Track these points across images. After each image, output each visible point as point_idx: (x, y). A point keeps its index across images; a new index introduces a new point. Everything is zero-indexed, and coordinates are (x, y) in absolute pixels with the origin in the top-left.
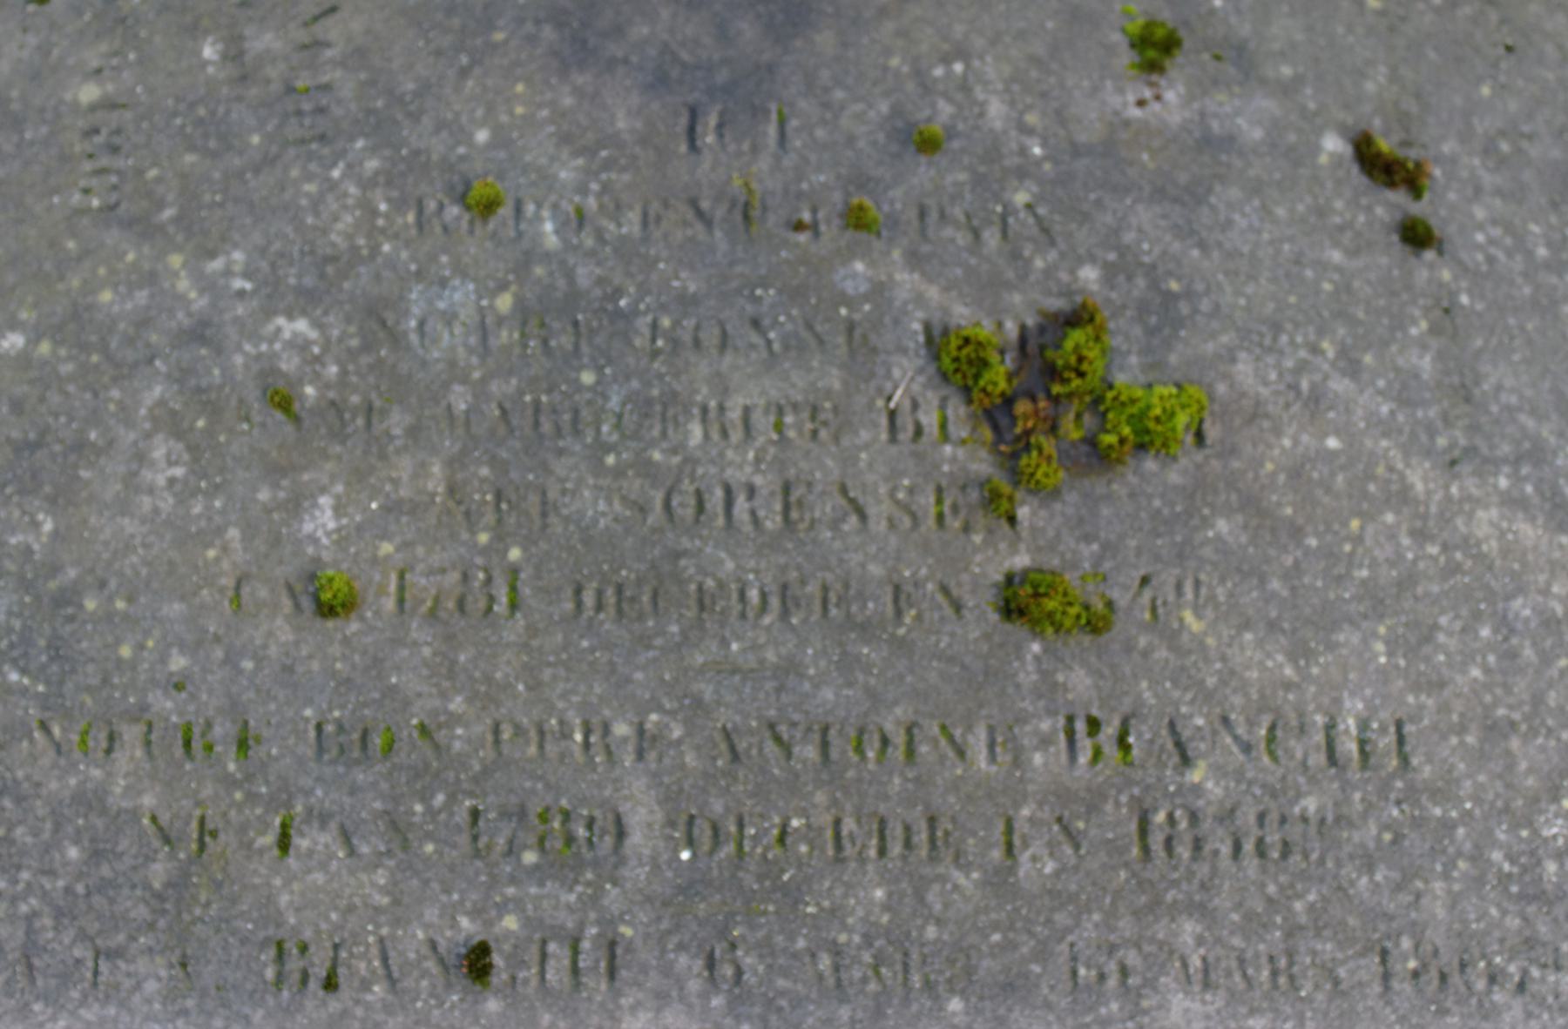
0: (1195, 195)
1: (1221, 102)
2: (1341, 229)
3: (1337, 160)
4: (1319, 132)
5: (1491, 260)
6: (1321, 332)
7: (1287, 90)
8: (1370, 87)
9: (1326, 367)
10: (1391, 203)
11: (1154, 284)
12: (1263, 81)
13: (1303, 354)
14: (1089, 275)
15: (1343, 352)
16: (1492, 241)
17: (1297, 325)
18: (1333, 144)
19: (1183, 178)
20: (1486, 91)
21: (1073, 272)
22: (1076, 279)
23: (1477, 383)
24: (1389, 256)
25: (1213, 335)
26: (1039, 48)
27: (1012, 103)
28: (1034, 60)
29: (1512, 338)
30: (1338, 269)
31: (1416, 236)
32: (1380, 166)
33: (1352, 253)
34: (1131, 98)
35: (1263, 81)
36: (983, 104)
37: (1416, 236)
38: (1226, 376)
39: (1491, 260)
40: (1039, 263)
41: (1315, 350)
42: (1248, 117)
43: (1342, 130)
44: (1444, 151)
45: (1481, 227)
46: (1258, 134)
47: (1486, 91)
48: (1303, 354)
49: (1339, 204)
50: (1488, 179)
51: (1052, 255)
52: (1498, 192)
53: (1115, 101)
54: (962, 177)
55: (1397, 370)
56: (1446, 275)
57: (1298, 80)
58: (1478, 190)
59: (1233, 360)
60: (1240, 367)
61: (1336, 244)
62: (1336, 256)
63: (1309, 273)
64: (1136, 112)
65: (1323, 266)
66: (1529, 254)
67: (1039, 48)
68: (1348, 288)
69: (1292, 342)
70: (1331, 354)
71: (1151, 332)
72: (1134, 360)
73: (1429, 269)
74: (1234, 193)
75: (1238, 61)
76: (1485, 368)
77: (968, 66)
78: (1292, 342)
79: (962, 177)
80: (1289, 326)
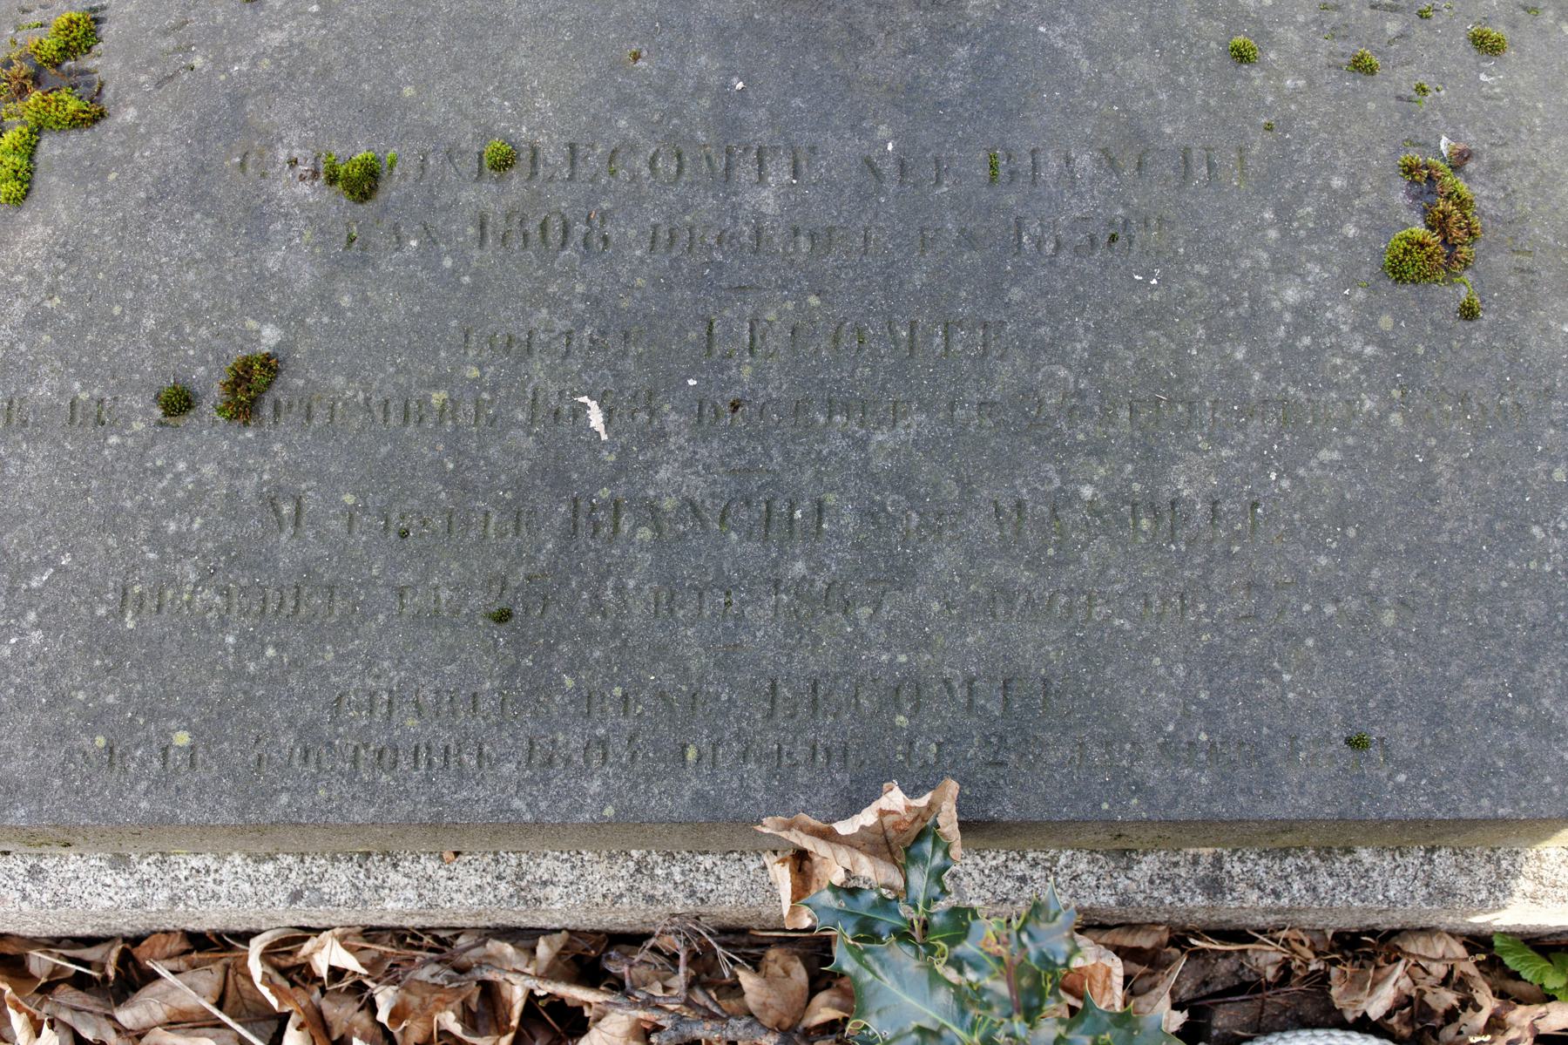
0: (198, 199)
1: (304, 236)
2: (178, 330)
3: (253, 337)
4: (281, 322)
5: (159, 472)
6: (68, 297)
7: (325, 299)
8: (339, 381)
9: (36, 299)
10: (209, 381)
11: (117, 162)
12: (330, 277)
13: (48, 279)
14: (130, 114)
15: (49, 316)
16: (178, 477)
17: (76, 277)
18: (270, 337)
19: (218, 191)
20: (349, 499)
21: (133, 103)
22: (126, 106)
23: (27, 439)
24: (154, 373)
25: (68, 208)
26: (340, 75)
27: (281, 50)
28: (327, 71)
29: (77, 480)
30: (136, 323)
31: (179, 403)
32: (251, 387)
33: (153, 337)
34: (296, 153)
35: (330, 277)
36: (281, 28)
37: (179, 403)
38: (33, 220)
39: (159, 472)
40: (143, 78)
41: (52, 290)
42: (291, 257)
43: (286, 346)
44: (272, 450)
45: (193, 468)
46: (272, 264)
47: (349, 499)
48: (48, 279)
49: (204, 332)
50: (249, 485)
51: (148, 88)
52: (233, 496)
53: (293, 136)
54: (220, 19)
55: (36, 363)
56: (138, 426)
57: (338, 312)
58: (235, 473)
59: (46, 224)
60: (40, 228)
61: (162, 325)
62: (149, 323)
63: (129, 295)
64: (282, 155)
65: (138, 308)
66: (169, 514)
67: (340, 75)
68: (115, 329)
69: (59, 272)
70: (48, 304)
71: (78, 161)
72: (57, 152)
73: (143, 415)
74: (207, 236)
75: (354, 252)
76: (44, 447)
77: (316, 15)
78: (59, 272)
79: (220, 19)
80: (74, 270)
